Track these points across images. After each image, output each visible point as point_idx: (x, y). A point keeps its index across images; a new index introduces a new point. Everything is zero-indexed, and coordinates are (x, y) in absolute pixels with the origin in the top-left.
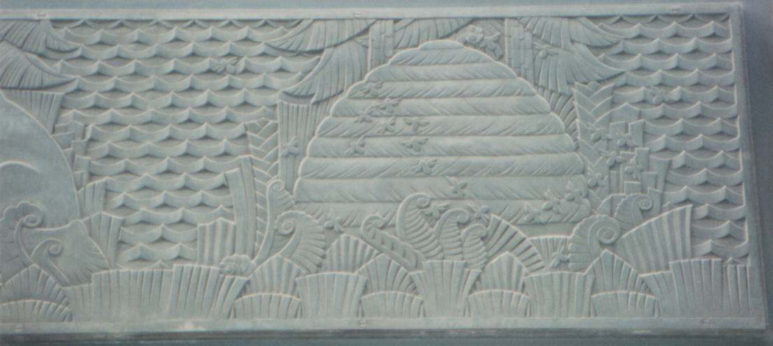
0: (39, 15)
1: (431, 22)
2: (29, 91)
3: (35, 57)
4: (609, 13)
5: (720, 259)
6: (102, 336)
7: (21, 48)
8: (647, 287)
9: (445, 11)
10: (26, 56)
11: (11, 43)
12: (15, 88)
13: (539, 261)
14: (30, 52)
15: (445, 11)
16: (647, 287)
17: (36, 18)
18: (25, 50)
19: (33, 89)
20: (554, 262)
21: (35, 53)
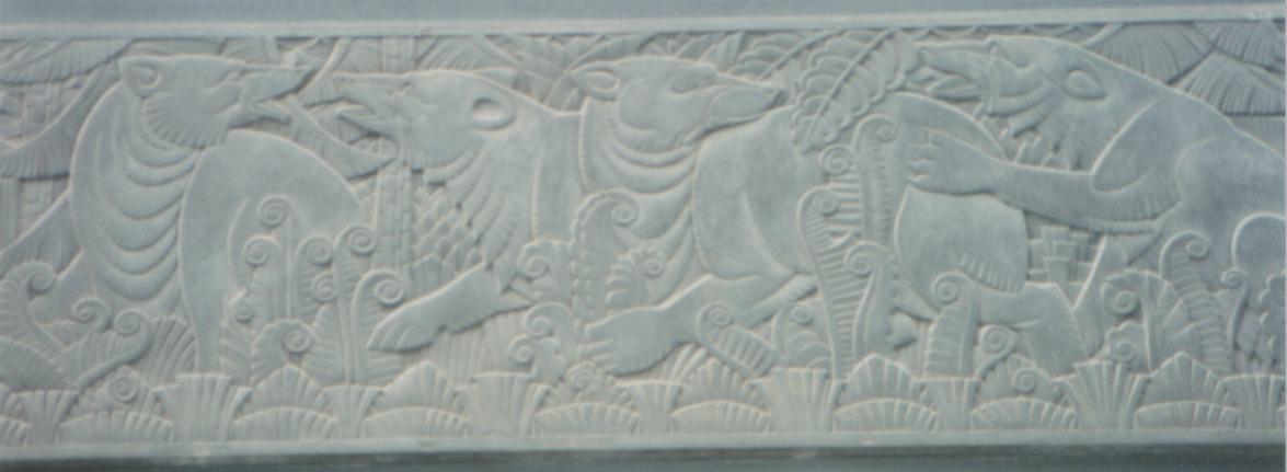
0: (1256, 13)
1: (373, 44)
2: (1263, 118)
3: (1262, 71)
4: (962, 23)
5: (1085, 236)
6: (185, 462)
7: (1240, 59)
8: (1030, 264)
9: (601, 26)
10: (1251, 71)
11: (1226, 53)
12: (1246, 114)
13: (823, 262)
14: (1253, 63)
15: (601, 26)
16: (1030, 264)
17: (1253, 16)
18: (1247, 62)
19: (1268, 114)
20: (184, 296)
21: (1262, 66)
